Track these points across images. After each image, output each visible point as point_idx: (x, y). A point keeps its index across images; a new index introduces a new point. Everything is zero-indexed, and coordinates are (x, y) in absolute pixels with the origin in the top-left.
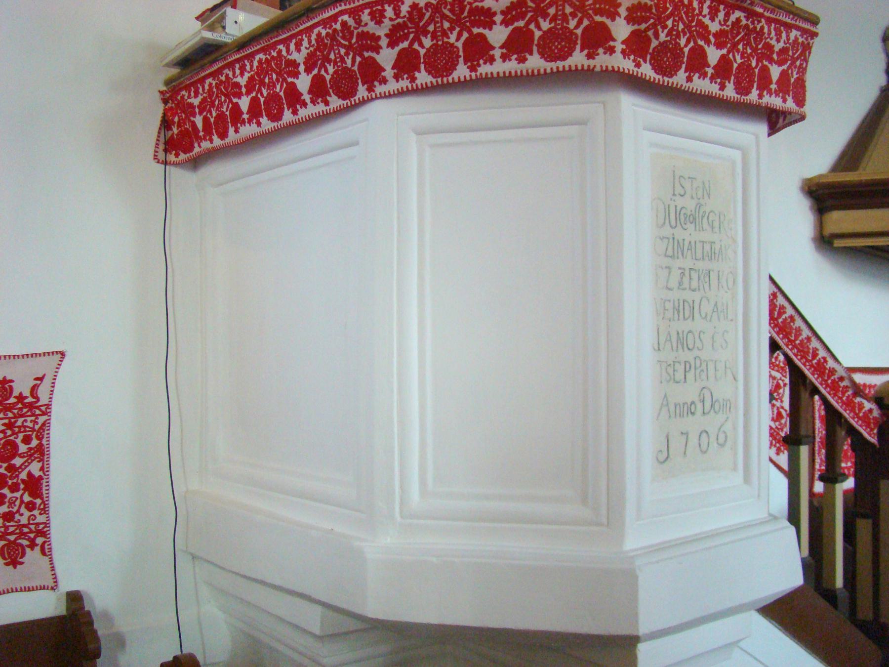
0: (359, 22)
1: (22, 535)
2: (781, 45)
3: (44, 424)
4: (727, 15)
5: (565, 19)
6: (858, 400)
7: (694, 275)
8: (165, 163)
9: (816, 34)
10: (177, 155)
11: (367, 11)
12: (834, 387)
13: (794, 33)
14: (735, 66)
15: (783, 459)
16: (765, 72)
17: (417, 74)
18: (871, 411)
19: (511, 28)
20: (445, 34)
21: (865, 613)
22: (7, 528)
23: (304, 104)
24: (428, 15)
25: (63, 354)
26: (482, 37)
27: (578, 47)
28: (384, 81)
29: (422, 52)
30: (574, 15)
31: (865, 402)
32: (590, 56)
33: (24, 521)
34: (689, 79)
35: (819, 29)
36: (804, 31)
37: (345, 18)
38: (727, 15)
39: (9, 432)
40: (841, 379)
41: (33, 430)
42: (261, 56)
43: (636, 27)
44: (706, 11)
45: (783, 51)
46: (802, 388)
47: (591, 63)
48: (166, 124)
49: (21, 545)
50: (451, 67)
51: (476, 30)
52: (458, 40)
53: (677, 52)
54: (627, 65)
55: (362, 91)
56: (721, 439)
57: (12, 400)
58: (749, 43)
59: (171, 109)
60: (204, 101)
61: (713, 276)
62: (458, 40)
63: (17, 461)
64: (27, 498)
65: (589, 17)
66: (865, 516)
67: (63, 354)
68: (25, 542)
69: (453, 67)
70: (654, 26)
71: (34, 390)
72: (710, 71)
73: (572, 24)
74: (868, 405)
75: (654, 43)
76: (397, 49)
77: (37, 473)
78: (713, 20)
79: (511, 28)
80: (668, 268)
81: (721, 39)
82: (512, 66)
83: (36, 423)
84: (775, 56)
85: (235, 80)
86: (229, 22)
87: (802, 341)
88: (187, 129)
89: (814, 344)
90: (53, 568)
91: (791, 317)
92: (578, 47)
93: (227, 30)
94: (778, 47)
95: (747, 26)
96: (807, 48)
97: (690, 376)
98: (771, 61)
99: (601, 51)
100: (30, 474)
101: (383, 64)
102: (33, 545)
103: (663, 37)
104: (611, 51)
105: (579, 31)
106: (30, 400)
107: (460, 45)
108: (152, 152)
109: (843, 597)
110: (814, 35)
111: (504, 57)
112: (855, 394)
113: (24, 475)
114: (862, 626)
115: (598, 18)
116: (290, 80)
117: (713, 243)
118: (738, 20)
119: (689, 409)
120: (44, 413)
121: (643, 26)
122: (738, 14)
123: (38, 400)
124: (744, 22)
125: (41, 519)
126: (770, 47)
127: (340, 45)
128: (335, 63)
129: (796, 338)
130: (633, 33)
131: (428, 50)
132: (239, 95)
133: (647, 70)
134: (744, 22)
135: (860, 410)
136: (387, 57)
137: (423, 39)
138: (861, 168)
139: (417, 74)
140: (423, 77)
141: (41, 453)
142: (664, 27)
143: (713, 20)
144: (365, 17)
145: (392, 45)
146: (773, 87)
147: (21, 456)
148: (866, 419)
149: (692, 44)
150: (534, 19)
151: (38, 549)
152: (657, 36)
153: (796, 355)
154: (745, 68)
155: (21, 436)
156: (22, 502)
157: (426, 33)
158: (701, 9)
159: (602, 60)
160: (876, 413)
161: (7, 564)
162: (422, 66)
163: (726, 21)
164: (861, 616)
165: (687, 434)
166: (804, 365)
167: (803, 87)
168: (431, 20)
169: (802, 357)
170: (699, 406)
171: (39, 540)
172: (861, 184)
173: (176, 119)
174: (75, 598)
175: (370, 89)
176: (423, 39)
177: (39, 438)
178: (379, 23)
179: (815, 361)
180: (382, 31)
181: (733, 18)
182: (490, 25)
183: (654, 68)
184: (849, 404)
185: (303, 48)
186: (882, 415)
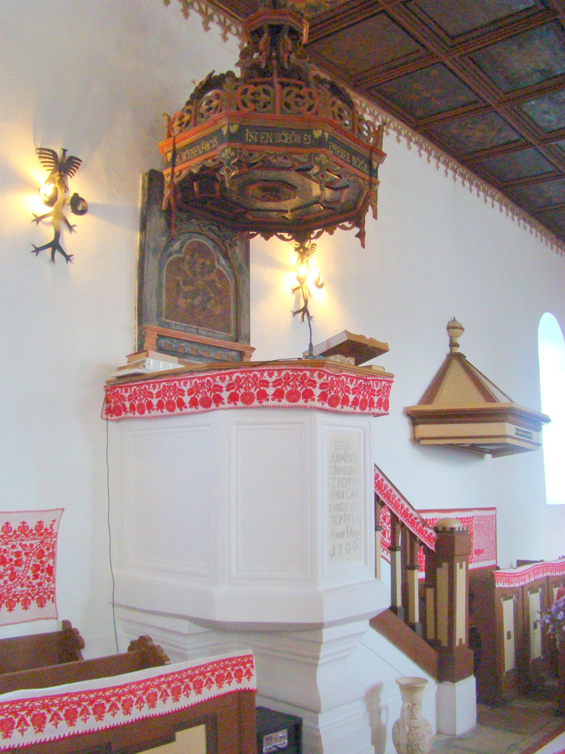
0: (215, 381)
1: (45, 593)
2: (378, 388)
3: (55, 542)
4: (357, 382)
5: (296, 386)
6: (425, 528)
7: (344, 481)
8: (107, 419)
9: (393, 381)
10: (112, 416)
11: (218, 377)
12: (412, 522)
13: (383, 383)
14: (360, 400)
15: (388, 557)
16: (372, 400)
17: (237, 402)
18: (431, 534)
19: (275, 388)
20: (249, 388)
21: (431, 635)
22: (39, 589)
23: (186, 407)
24: (243, 381)
25: (63, 510)
26: (265, 391)
27: (301, 398)
28: (223, 403)
29: (240, 394)
30: (299, 385)
31: (428, 530)
32: (306, 402)
33: (46, 586)
34: (342, 407)
35: (394, 379)
36: (387, 381)
37: (209, 378)
38: (357, 382)
39: (41, 545)
40: (416, 518)
41: (51, 544)
42: (165, 383)
43: (323, 390)
44: (349, 381)
45: (380, 390)
46: (397, 523)
47: (306, 404)
48: (107, 401)
49: (44, 598)
50: (251, 401)
51: (262, 388)
52: (255, 391)
53: (337, 398)
54: (319, 405)
55: (213, 406)
56: (355, 546)
57: (43, 531)
58: (365, 390)
59: (110, 395)
60: (131, 395)
61: (352, 481)
62: (255, 391)
63: (44, 559)
64: (47, 576)
65: (306, 387)
66: (431, 587)
67: (63, 510)
68: (46, 596)
69: (253, 401)
70: (329, 390)
71: (51, 526)
72: (350, 404)
73: (299, 389)
74: (430, 531)
75: (329, 396)
76: (230, 392)
77: (51, 565)
78: (351, 384)
79: (275, 388)
80: (334, 479)
81: (354, 391)
82: (276, 403)
83: (51, 541)
84: (376, 393)
85: (150, 390)
86: (146, 364)
87: (396, 501)
88: (118, 406)
89: (402, 502)
90: (56, 609)
91: (391, 490)
92: (301, 398)
93: (146, 367)
94: (377, 389)
95: (364, 385)
96: (389, 387)
97: (342, 521)
98: (374, 395)
99: (310, 400)
100: (49, 565)
101: (223, 397)
102: (49, 598)
103: (332, 393)
104: (314, 400)
105: (302, 392)
106: (49, 531)
107: (255, 393)
108: (100, 415)
109: (419, 627)
110: (391, 382)
111: (273, 399)
112: (423, 526)
113: (46, 566)
114: (429, 642)
115: (309, 387)
116: (180, 397)
117: (351, 467)
118: (361, 383)
119: (342, 535)
120: (55, 537)
121: (325, 390)
122: (361, 381)
123: (53, 530)
124: (363, 383)
125: (52, 586)
126: (374, 390)
127: (205, 387)
128: (202, 394)
129: (393, 499)
130: (322, 393)
131: (242, 394)
132: (152, 397)
133: (326, 406)
134: (363, 383)
135: (426, 534)
136: (225, 395)
137: (241, 389)
138: (435, 402)
139: (237, 402)
140: (240, 403)
141: (53, 555)
142: (333, 390)
143: (351, 384)
144: (218, 379)
145: (228, 390)
146: (375, 405)
147: (46, 556)
148: (429, 538)
149: (343, 395)
150: (284, 386)
151: (51, 600)
152: (330, 393)
153: (393, 508)
154: (364, 400)
155: (46, 547)
156: (45, 578)
157: (242, 387)
158: (346, 382)
159: (310, 403)
160: (434, 535)
161: (39, 606)
162: (240, 400)
163: (356, 384)
164: (428, 637)
165: (341, 545)
166: (397, 512)
167: (388, 403)
168: (293, 379)
169: (396, 509)
170: (346, 533)
171: (52, 596)
172: (433, 412)
173: (113, 400)
174: (66, 624)
175: (217, 406)
176: (241, 389)
177: (53, 548)
178: (223, 382)
179: (402, 510)
180: (224, 385)
181: (359, 382)
182: (267, 386)
183: (329, 404)
184: (421, 531)
185: (187, 385)
186: (438, 536)
